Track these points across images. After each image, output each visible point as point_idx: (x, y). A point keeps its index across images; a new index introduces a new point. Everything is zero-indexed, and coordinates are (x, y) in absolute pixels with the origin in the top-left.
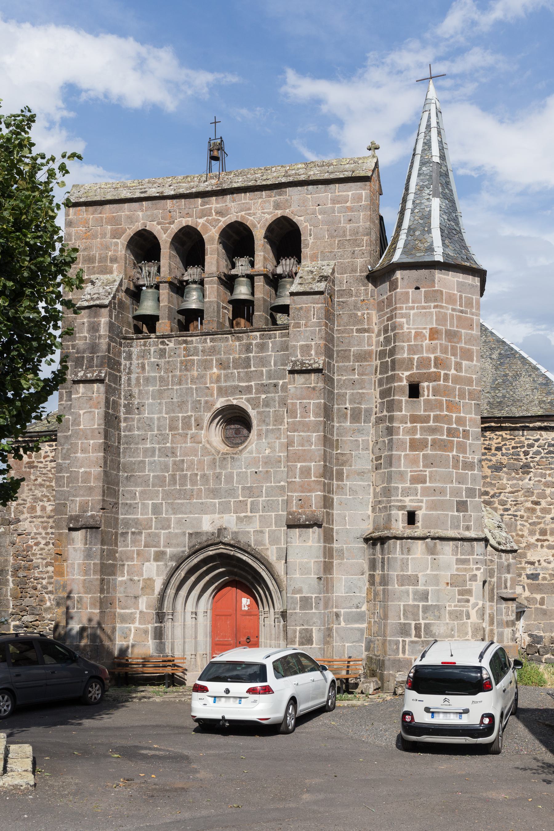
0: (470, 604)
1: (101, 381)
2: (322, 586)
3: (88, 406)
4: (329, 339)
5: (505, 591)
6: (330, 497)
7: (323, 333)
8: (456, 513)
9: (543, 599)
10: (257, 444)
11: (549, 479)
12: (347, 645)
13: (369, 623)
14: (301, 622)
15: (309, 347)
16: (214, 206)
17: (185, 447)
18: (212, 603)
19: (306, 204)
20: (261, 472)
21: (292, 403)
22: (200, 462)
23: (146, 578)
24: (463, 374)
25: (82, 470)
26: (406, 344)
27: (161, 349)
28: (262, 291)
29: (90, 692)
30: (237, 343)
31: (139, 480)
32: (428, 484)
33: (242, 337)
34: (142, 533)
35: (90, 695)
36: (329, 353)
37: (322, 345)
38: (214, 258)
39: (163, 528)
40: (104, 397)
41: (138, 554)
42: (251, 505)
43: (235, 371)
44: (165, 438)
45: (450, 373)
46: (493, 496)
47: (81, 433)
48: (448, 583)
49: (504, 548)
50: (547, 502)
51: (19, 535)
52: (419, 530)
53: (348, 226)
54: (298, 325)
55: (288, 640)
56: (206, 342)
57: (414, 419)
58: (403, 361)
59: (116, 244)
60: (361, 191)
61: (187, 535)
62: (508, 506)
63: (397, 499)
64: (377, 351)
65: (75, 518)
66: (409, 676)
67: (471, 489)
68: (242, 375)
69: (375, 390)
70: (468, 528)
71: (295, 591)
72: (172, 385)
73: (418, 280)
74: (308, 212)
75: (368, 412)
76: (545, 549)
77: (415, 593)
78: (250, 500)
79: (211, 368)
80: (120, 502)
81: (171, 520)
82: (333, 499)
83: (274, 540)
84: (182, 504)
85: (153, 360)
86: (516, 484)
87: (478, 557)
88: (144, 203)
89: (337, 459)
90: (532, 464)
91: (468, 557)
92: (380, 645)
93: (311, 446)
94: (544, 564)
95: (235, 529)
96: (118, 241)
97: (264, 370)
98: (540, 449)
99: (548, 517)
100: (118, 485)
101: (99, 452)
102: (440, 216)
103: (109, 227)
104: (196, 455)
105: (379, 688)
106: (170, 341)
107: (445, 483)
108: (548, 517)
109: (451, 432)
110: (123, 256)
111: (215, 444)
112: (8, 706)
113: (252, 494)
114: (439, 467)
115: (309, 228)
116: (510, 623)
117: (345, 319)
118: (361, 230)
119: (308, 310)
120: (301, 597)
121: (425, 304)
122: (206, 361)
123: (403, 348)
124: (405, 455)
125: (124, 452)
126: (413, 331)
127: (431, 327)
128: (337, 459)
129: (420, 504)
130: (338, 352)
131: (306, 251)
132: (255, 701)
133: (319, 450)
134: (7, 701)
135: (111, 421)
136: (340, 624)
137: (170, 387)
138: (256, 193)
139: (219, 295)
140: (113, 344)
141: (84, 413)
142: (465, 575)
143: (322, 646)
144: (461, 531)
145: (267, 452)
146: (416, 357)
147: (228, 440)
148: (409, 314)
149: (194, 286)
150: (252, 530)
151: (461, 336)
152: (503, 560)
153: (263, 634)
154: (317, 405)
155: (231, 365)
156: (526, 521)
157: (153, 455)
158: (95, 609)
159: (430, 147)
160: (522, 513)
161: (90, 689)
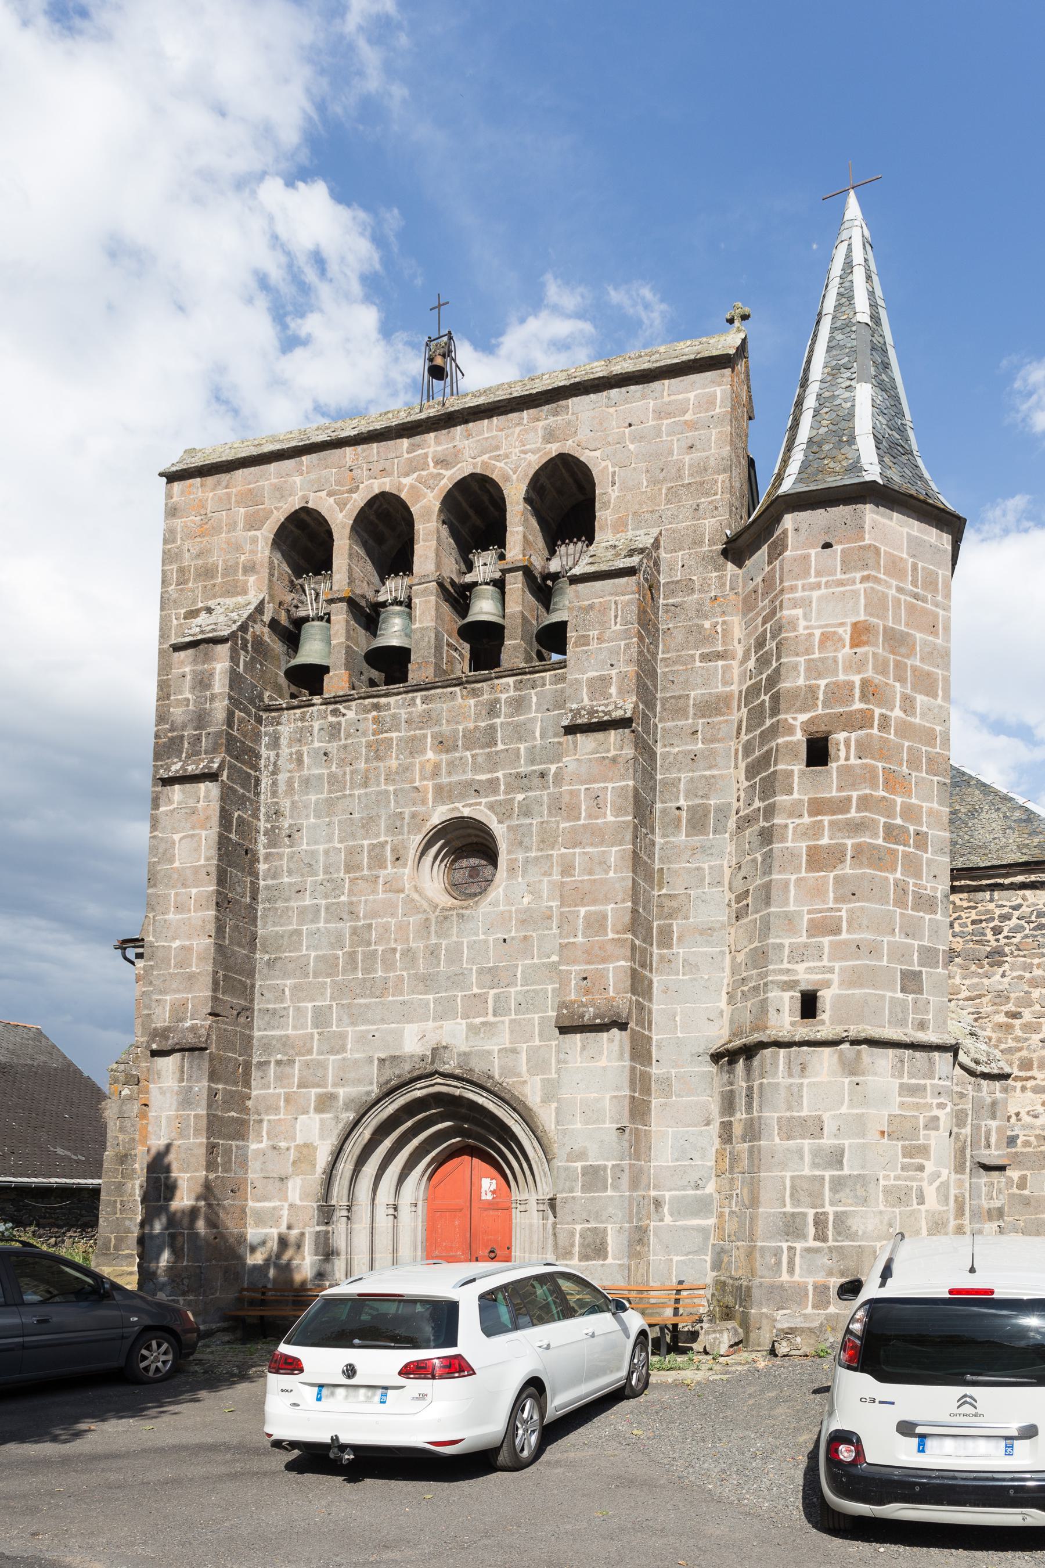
0: (925, 1175)
1: (211, 776)
2: (626, 1145)
3: (189, 825)
5: (987, 1152)
6: (646, 977)
7: (634, 651)
8: (900, 995)
9: (1023, 1179)
10: (507, 886)
11: (1038, 972)
12: (676, 1258)
13: (721, 1215)
14: (585, 1216)
15: (604, 681)
16: (431, 450)
17: (374, 901)
18: (426, 1188)
19: (605, 425)
20: (513, 938)
21: (571, 792)
22: (402, 927)
23: (302, 1143)
24: (917, 721)
25: (176, 944)
26: (801, 659)
27: (331, 725)
28: (520, 600)
29: (144, 1358)
30: (472, 702)
31: (290, 966)
32: (844, 936)
33: (481, 689)
34: (294, 1062)
35: (143, 1365)
38: (431, 547)
39: (332, 1051)
41: (287, 1101)
42: (495, 1002)
43: (468, 754)
44: (336, 886)
47: (175, 876)
48: (883, 1133)
49: (986, 1071)
50: (1033, 1013)
52: (825, 1026)
53: (687, 458)
55: (560, 1251)
56: (415, 704)
57: (817, 807)
58: (795, 693)
59: (254, 540)
61: (376, 1062)
63: (779, 968)
64: (741, 692)
65: (162, 1034)
66: (848, 1331)
67: (929, 950)
68: (480, 759)
70: (922, 1026)
71: (572, 1157)
73: (828, 530)
74: (610, 439)
75: (722, 811)
76: (1029, 1094)
77: (816, 1153)
78: (492, 992)
79: (423, 751)
80: (256, 1007)
81: (346, 1037)
82: (651, 982)
83: (537, 1066)
84: (367, 1006)
85: (316, 745)
86: (977, 984)
87: (941, 1082)
88: (304, 458)
89: (661, 906)
90: (1007, 949)
91: (922, 1082)
93: (607, 873)
94: (1026, 1119)
95: (464, 1048)
98: (1022, 922)
99: (1036, 1038)
100: (251, 974)
101: (208, 909)
102: (873, 415)
103: (242, 510)
105: (741, 1342)
106: (349, 708)
108: (1036, 1038)
109: (891, 833)
110: (267, 560)
111: (430, 894)
112: (164, 1362)
113: (496, 981)
114: (868, 900)
115: (611, 470)
116: (995, 1213)
117: (679, 636)
118: (712, 462)
119: (604, 609)
120: (583, 1168)
121: (844, 577)
122: (413, 738)
123: (795, 667)
125: (265, 916)
126: (817, 633)
127: (854, 620)
129: (828, 976)
130: (665, 700)
132: (422, 1397)
133: (623, 879)
134: (165, 1353)
136: (662, 1220)
137: (348, 792)
138: (510, 416)
139: (439, 617)
141: (181, 839)
142: (917, 1117)
143: (625, 1261)
144: (910, 1030)
145: (526, 900)
146: (822, 683)
147: (456, 889)
149: (397, 608)
150: (496, 1048)
151: (914, 644)
152: (984, 1094)
153: (518, 1241)
154: (621, 792)
155: (460, 743)
156: (996, 1047)
157: (315, 919)
159: (850, 298)
160: (988, 1033)
161: (144, 1352)
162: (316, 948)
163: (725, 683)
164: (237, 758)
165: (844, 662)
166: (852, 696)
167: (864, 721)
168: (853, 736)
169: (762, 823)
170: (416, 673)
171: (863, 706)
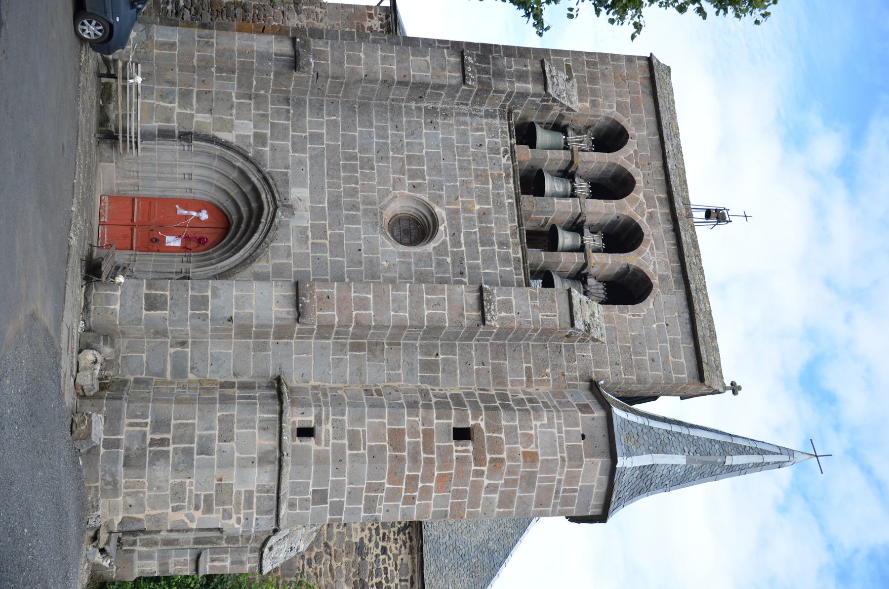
0: (192, 511)
4: (520, 334)
6: (330, 334)
7: (526, 326)
8: (311, 490)
12: (144, 356)
13: (172, 383)
14: (175, 297)
15: (509, 309)
20: (361, 255)
21: (444, 290)
22: (371, 188)
24: (483, 495)
25: (362, 55)
26: (517, 423)
27: (498, 149)
29: (90, 22)
30: (508, 232)
32: (348, 452)
35: (86, 22)
36: (503, 333)
37: (512, 325)
39: (293, 143)
40: (444, 83)
41: (263, 115)
45: (484, 479)
46: (326, 545)
48: (221, 480)
51: (283, 12)
53: (647, 358)
54: (534, 297)
55: (153, 282)
56: (508, 198)
57: (428, 435)
58: (497, 419)
59: (611, 107)
60: (686, 373)
62: (314, 565)
63: (330, 414)
65: (306, 45)
67: (342, 509)
68: (473, 236)
69: (461, 388)
70: (292, 505)
72: (459, 160)
75: (434, 381)
77: (210, 438)
78: (327, 242)
79: (479, 203)
85: (487, 140)
91: (254, 506)
92: (142, 396)
96: (615, 109)
97: (480, 261)
103: (629, 100)
104: (379, 183)
106: (508, 160)
107: (350, 474)
109: (412, 480)
111: (392, 205)
117: (541, 354)
118: (644, 372)
119: (551, 309)
122: (488, 198)
123: (513, 420)
124: (384, 424)
126: (533, 432)
128: (377, 344)
129: (323, 443)
130: (503, 345)
131: (616, 309)
133: (389, 320)
134: (95, 34)
135: (420, 89)
140: (504, 96)
142: (231, 504)
145: (385, 263)
146: (503, 436)
148: (554, 428)
149: (570, 189)
150: (291, 244)
157: (378, 136)
158: (198, 60)
159: (740, 453)
161: (94, 22)
162: (360, 136)
163: (512, 381)
164: (476, 94)
165: (515, 448)
166: (494, 453)
167: (479, 461)
168: (471, 454)
169: (421, 403)
170: (528, 200)
171: (488, 459)
